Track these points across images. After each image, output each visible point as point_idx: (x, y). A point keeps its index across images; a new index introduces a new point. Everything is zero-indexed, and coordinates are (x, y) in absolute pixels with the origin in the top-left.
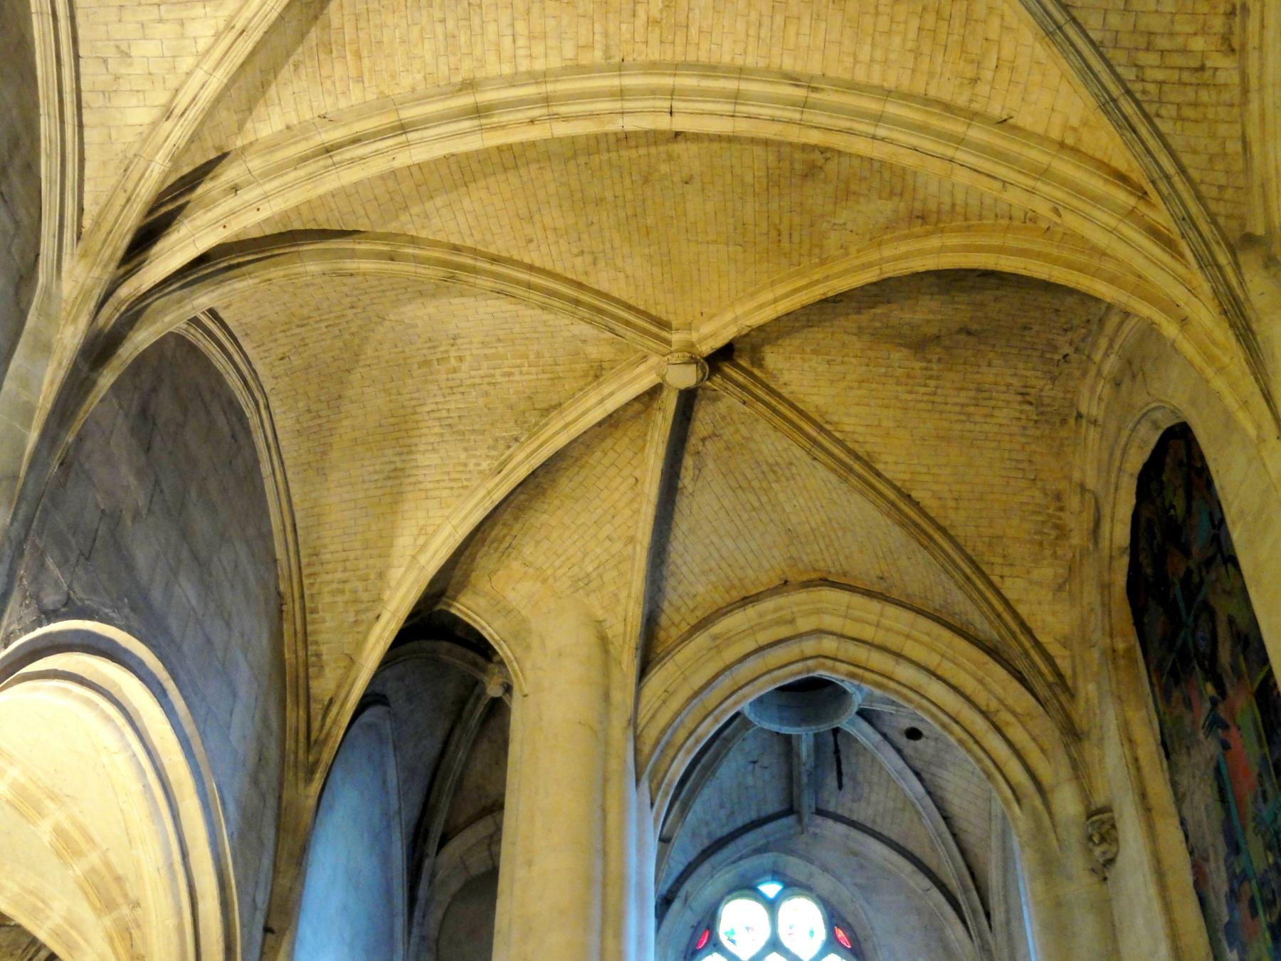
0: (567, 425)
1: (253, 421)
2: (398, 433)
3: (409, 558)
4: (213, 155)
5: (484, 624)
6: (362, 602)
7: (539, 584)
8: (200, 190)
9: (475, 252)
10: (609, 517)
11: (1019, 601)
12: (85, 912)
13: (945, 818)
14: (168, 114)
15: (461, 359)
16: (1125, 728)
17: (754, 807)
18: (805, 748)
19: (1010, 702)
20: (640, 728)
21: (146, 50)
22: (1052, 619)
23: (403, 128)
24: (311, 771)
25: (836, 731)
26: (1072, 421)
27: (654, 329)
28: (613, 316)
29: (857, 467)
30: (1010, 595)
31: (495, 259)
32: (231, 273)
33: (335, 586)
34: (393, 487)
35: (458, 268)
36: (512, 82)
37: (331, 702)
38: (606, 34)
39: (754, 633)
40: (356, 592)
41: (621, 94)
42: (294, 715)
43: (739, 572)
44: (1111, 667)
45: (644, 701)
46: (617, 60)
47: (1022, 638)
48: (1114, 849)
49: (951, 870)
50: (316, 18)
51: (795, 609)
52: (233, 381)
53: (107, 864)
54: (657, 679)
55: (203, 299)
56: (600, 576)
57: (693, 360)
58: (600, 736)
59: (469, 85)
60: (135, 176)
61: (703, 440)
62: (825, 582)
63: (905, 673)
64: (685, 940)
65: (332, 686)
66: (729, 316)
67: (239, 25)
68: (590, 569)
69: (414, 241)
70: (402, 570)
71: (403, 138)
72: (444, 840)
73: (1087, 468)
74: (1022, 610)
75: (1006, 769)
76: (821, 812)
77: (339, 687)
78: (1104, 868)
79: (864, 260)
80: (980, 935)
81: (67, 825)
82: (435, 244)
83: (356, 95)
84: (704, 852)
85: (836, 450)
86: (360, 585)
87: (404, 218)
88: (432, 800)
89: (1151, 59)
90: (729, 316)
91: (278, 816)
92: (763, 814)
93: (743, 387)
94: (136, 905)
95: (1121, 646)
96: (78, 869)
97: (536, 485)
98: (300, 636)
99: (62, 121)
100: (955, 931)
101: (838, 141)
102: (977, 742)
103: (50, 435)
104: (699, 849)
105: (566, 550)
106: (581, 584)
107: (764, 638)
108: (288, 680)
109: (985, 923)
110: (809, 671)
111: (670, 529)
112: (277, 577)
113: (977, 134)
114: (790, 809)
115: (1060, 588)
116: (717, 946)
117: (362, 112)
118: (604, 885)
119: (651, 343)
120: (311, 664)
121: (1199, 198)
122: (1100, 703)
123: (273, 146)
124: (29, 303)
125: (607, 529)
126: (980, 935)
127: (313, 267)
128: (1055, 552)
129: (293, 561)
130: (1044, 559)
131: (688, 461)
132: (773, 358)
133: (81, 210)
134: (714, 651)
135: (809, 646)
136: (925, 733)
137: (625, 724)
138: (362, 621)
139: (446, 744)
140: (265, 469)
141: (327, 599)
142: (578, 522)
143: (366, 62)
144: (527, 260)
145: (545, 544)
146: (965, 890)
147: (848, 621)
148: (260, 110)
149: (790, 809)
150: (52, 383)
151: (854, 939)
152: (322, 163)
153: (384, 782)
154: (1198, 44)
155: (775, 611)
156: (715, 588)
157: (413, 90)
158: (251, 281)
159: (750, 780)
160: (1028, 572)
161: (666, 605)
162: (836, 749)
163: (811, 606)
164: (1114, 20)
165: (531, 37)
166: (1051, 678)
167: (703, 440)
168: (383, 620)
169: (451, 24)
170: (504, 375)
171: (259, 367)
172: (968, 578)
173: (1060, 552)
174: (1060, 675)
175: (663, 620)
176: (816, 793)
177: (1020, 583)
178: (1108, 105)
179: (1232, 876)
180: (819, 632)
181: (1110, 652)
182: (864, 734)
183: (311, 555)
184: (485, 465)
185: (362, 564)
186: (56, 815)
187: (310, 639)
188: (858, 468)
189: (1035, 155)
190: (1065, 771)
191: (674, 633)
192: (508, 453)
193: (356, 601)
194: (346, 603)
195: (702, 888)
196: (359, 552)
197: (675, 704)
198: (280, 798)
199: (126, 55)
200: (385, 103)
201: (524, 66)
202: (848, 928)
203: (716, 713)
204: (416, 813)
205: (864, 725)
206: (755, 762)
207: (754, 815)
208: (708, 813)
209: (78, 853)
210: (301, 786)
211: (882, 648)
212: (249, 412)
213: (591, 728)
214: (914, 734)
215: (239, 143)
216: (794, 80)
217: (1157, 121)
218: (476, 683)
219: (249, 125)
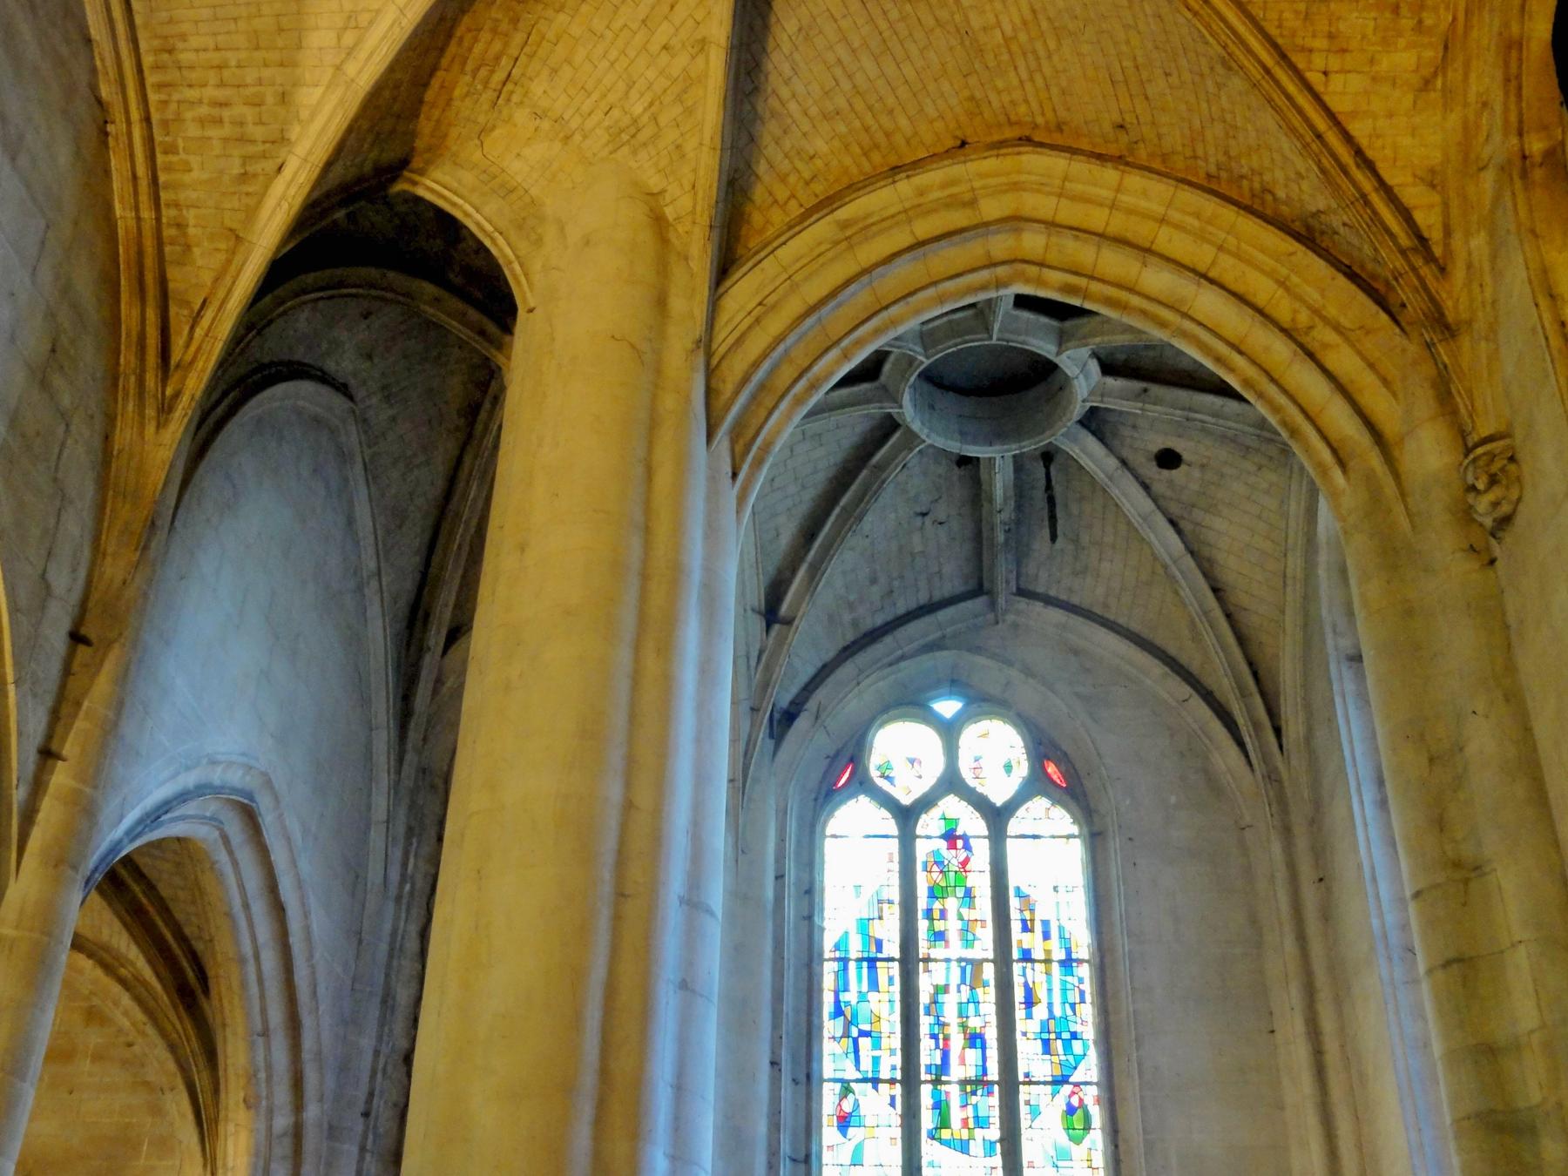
3: (330, 71)
5: (467, 207)
6: (253, 142)
7: (557, 145)
10: (666, 8)
11: (1354, 114)
13: (1216, 590)
17: (923, 584)
18: (1000, 482)
19: (1332, 311)
20: (714, 362)
22: (1409, 138)
30: (1338, 105)
33: (204, 110)
39: (910, 221)
40: (242, 124)
42: (136, 313)
43: (885, 121)
44: (1518, 184)
45: (723, 318)
47: (1358, 175)
48: (1514, 495)
49: (1221, 667)
51: (977, 184)
54: (743, 292)
56: (655, 119)
58: (648, 359)
63: (1158, 280)
64: (816, 776)
65: (207, 277)
68: (638, 109)
70: (319, 91)
74: (1358, 129)
75: (1324, 421)
76: (1022, 592)
80: (1266, 758)
84: (845, 649)
86: (249, 114)
88: (433, 570)
92: (937, 596)
100: (1226, 756)
102: (1273, 380)
104: (841, 644)
105: (600, 81)
106: (625, 137)
107: (925, 228)
111: (766, 27)
115: (1427, 84)
116: (861, 783)
118: (645, 577)
122: (1494, 257)
125: (663, 33)
126: (1266, 758)
128: (1420, 22)
130: (1400, 34)
134: (844, 245)
135: (1000, 245)
136: (1185, 456)
138: (255, 175)
139: (452, 480)
141: (193, 131)
142: (617, 25)
145: (567, 72)
146: (1243, 694)
147: (1064, 202)
149: (979, 588)
151: (1070, 772)
153: (350, 521)
155: (944, 186)
156: (847, 147)
159: (917, 543)
160: (1372, 61)
161: (762, 168)
163: (1003, 179)
166: (1405, 240)
168: (288, 172)
172: (1268, 71)
173: (1429, 21)
174: (1422, 240)
176: (1019, 563)
177: (1356, 82)
180: (1015, 222)
181: (1517, 161)
182: (1090, 456)
183: (157, 51)
185: (250, 76)
187: (164, 196)
190: (1424, 402)
191: (778, 218)
193: (242, 140)
194: (225, 140)
195: (845, 698)
196: (243, 55)
202: (1064, 760)
203: (845, 343)
204: (409, 585)
205: (1091, 442)
206: (924, 515)
207: (923, 598)
210: (150, 429)
211: (1120, 241)
213: (633, 346)
214: (1169, 459)
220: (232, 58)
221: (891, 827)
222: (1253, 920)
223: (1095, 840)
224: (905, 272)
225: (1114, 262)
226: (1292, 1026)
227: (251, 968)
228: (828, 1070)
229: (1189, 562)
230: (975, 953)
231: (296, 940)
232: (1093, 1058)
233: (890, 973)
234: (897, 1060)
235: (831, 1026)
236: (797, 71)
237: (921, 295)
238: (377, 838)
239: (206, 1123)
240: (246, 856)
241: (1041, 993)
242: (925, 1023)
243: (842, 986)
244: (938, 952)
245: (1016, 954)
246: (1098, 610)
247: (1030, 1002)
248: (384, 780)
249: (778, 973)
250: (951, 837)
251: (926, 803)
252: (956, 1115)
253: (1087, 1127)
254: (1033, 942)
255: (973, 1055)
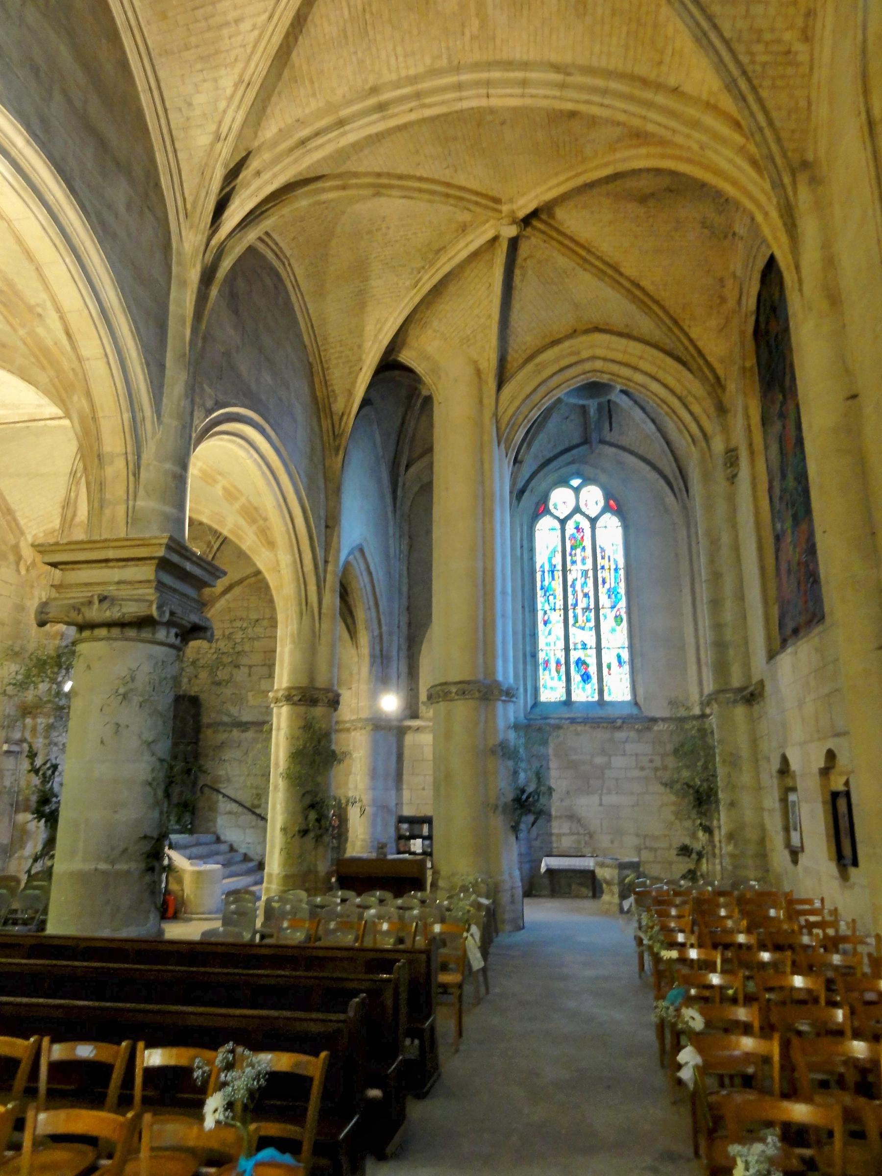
0: (450, 259)
1: (283, 274)
2: (360, 270)
4: (244, 154)
8: (241, 177)
9: (389, 175)
12: (242, 522)
14: (218, 138)
15: (388, 228)
16: (746, 408)
18: (592, 411)
21: (200, 99)
23: (341, 123)
24: (337, 449)
25: (609, 401)
26: (730, 236)
27: (491, 204)
28: (469, 201)
29: (610, 272)
30: (693, 336)
31: (401, 177)
32: (262, 217)
33: (337, 355)
34: (360, 302)
35: (382, 184)
36: (397, 85)
37: (343, 414)
38: (448, 48)
41: (459, 87)
46: (455, 63)
49: (669, 467)
50: (286, 63)
52: (270, 256)
53: (250, 502)
54: (507, 390)
55: (251, 236)
56: (475, 337)
57: (514, 222)
58: (478, 424)
59: (374, 90)
60: (208, 177)
61: (525, 259)
62: (597, 329)
63: (639, 378)
65: (343, 406)
66: (533, 194)
67: (247, 79)
68: (469, 333)
69: (356, 175)
70: (370, 343)
71: (342, 130)
72: (408, 467)
73: (737, 265)
74: (700, 344)
76: (602, 442)
77: (346, 406)
78: (732, 479)
79: (605, 160)
81: (228, 486)
82: (367, 174)
83: (314, 105)
85: (597, 263)
87: (348, 163)
89: (759, 48)
90: (533, 194)
91: (325, 473)
93: (544, 232)
94: (265, 520)
95: (748, 364)
96: (237, 506)
97: (437, 291)
98: (323, 383)
99: (166, 151)
100: (670, 499)
101: (582, 108)
103: (195, 330)
104: (540, 463)
107: (564, 363)
108: (321, 406)
109: (685, 495)
110: (588, 379)
112: (307, 355)
113: (660, 99)
114: (586, 441)
115: (721, 331)
116: (549, 512)
117: (319, 114)
119: (490, 213)
120: (330, 396)
121: (779, 140)
123: (274, 144)
124: (171, 261)
127: (304, 203)
129: (314, 345)
131: (517, 272)
132: (560, 213)
133: (184, 200)
135: (588, 366)
137: (491, 415)
140: (293, 298)
141: (334, 362)
143: (316, 85)
144: (418, 174)
146: (676, 479)
148: (264, 123)
149: (586, 441)
150: (191, 303)
152: (301, 151)
153: (375, 445)
154: (787, 36)
157: (344, 96)
158: (274, 219)
161: (510, 350)
162: (609, 411)
164: (740, 24)
165: (406, 56)
167: (525, 259)
169: (360, 54)
170: (412, 234)
171: (282, 244)
174: (718, 378)
175: (509, 358)
178: (731, 86)
179: (781, 491)
180: (594, 358)
184: (408, 283)
186: (222, 482)
187: (328, 383)
188: (610, 272)
189: (692, 112)
191: (515, 365)
192: (419, 276)
197: (517, 403)
198: (324, 465)
199: (190, 104)
200: (331, 108)
201: (403, 73)
202: (616, 500)
204: (392, 455)
205: (624, 397)
207: (567, 445)
208: (542, 446)
209: (236, 499)
212: (281, 270)
215: (256, 144)
216: (556, 68)
217: (760, 90)
218: (416, 389)
219: (260, 133)
220: (344, 338)
221: (557, 525)
222: (677, 555)
223: (626, 527)
224: (556, 380)
225: (626, 372)
226: (687, 591)
227: (364, 590)
228: (539, 606)
229: (658, 434)
230: (585, 568)
231: (375, 582)
232: (624, 598)
233: (559, 574)
234: (562, 602)
235: (540, 593)
236: (520, 319)
237: (563, 386)
238: (391, 541)
239: (352, 633)
240: (361, 561)
241: (608, 580)
242: (570, 590)
243: (543, 580)
244: (574, 568)
245: (599, 567)
246: (628, 447)
247: (604, 582)
248: (391, 523)
249: (523, 579)
250: (578, 529)
251: (569, 517)
252: (580, 618)
253: (622, 621)
254: (605, 563)
255: (585, 600)
